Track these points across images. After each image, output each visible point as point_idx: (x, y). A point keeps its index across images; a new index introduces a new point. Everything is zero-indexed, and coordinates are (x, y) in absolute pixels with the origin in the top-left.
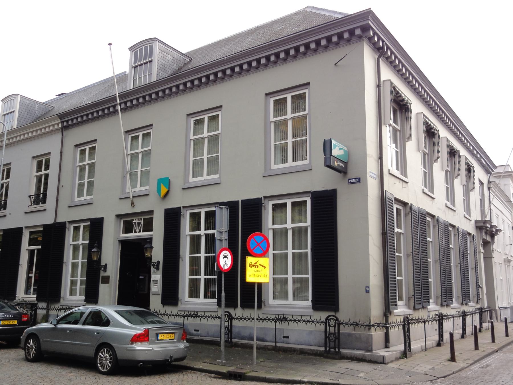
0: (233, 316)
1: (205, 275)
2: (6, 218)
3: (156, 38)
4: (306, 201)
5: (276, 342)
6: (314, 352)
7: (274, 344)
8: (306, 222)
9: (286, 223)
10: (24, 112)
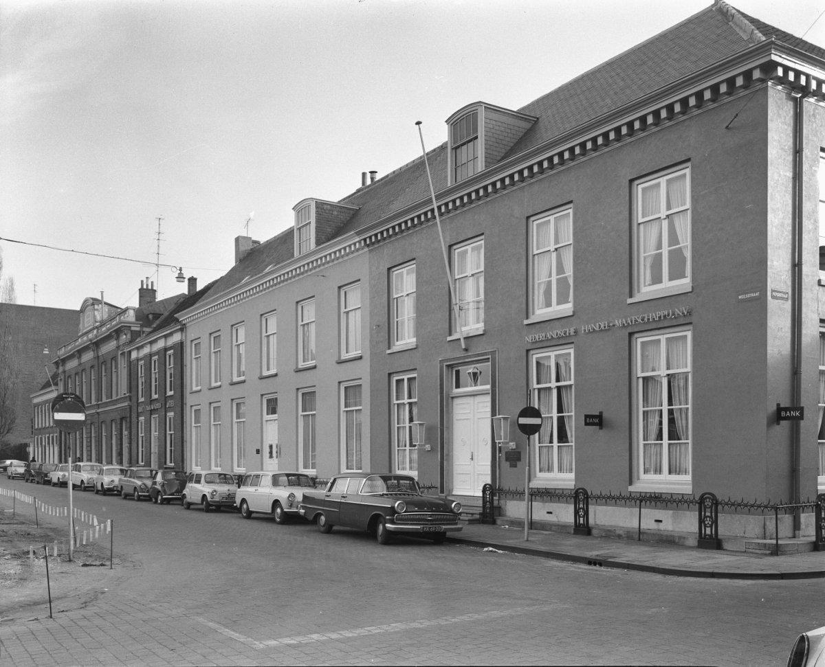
0: (589, 494)
1: (559, 442)
2: (317, 369)
3: (480, 102)
5: (777, 539)
6: (665, 538)
7: (774, 542)
8: (570, 380)
9: (550, 382)
10: (495, 153)
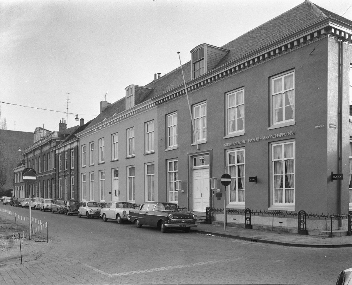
0: (252, 211)
1: (238, 189)
2: (135, 158)
3: (205, 44)
4: (293, 144)
5: (332, 230)
6: (284, 230)
7: (330, 231)
8: (243, 162)
9: (235, 163)
10: (211, 65)
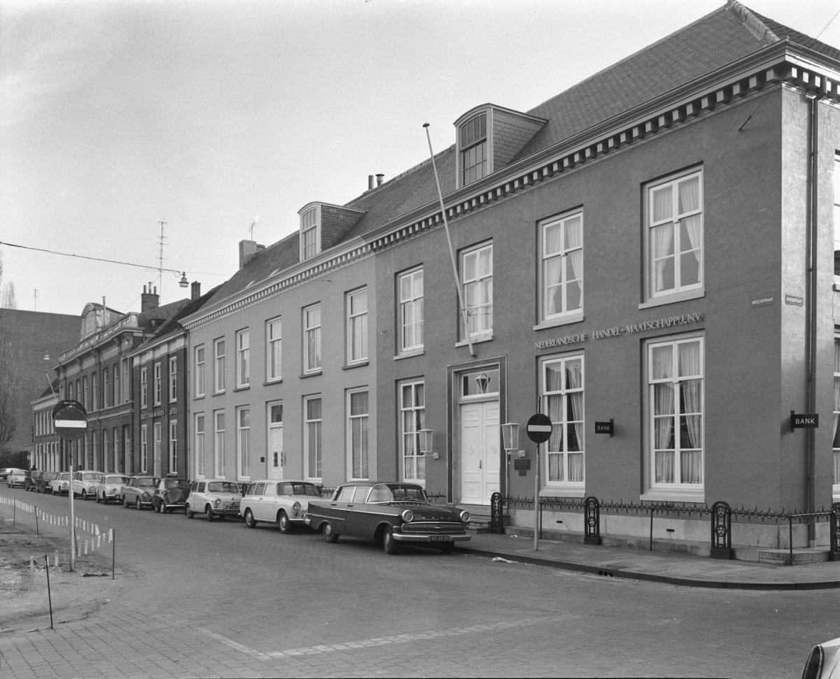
0: (600, 503)
1: (569, 450)
2: (323, 376)
3: (489, 104)
5: (791, 549)
6: (677, 548)
7: (788, 551)
8: (581, 387)
9: (560, 389)
10: (504, 156)
